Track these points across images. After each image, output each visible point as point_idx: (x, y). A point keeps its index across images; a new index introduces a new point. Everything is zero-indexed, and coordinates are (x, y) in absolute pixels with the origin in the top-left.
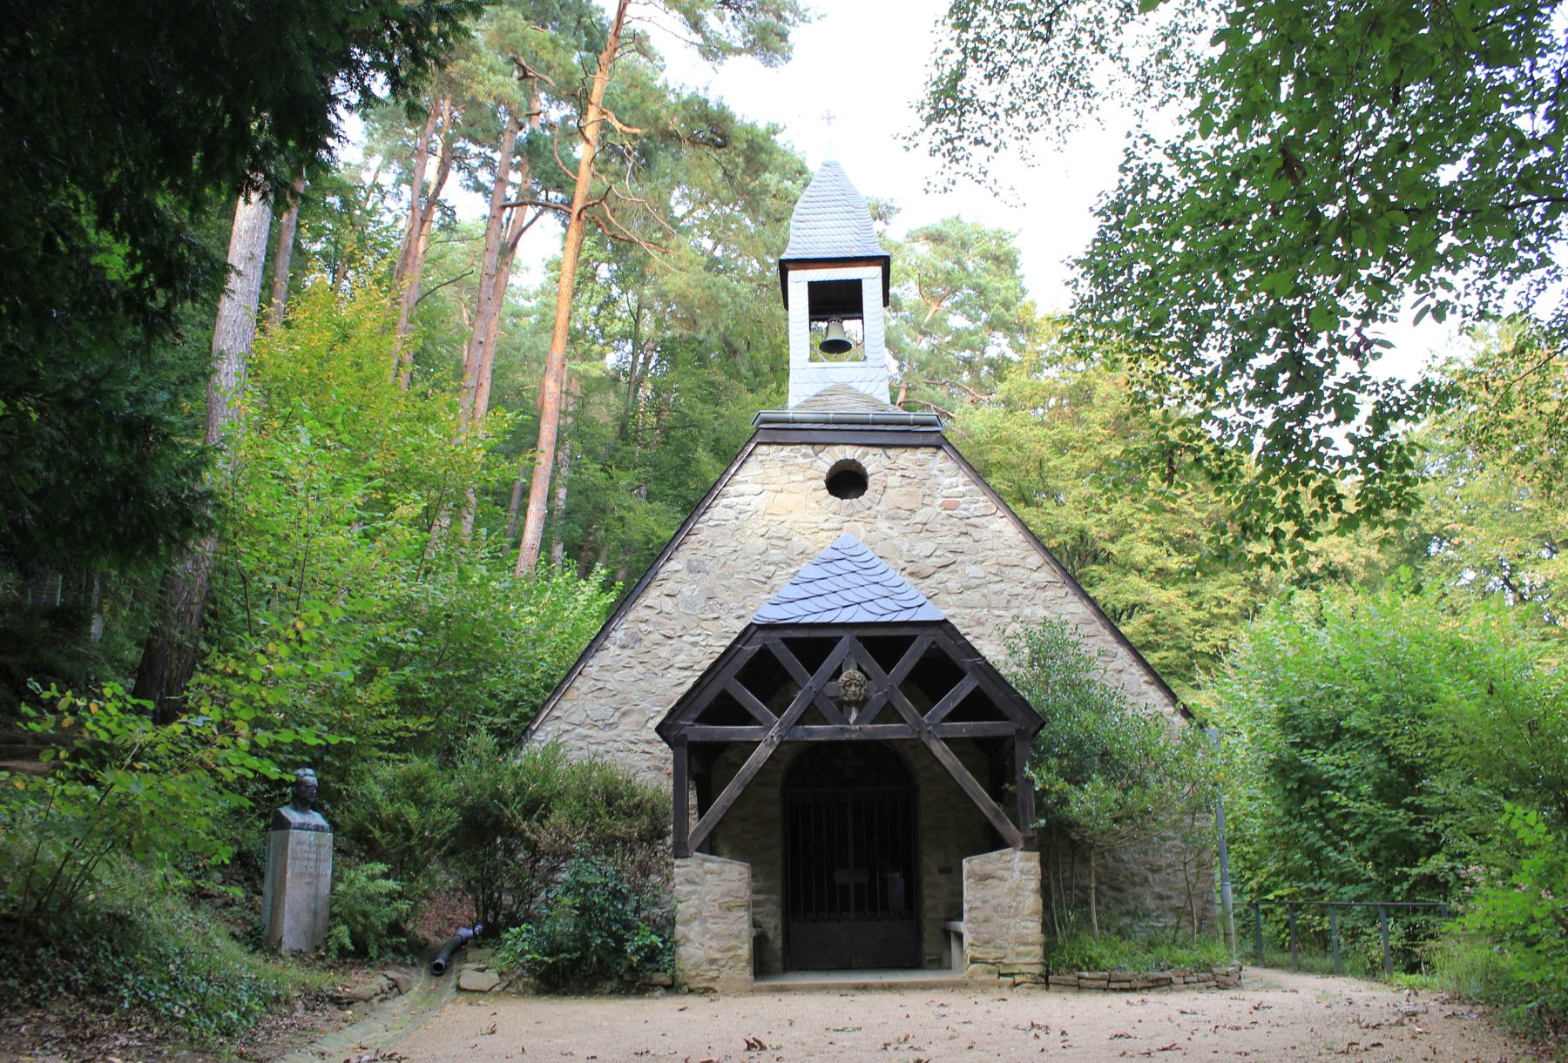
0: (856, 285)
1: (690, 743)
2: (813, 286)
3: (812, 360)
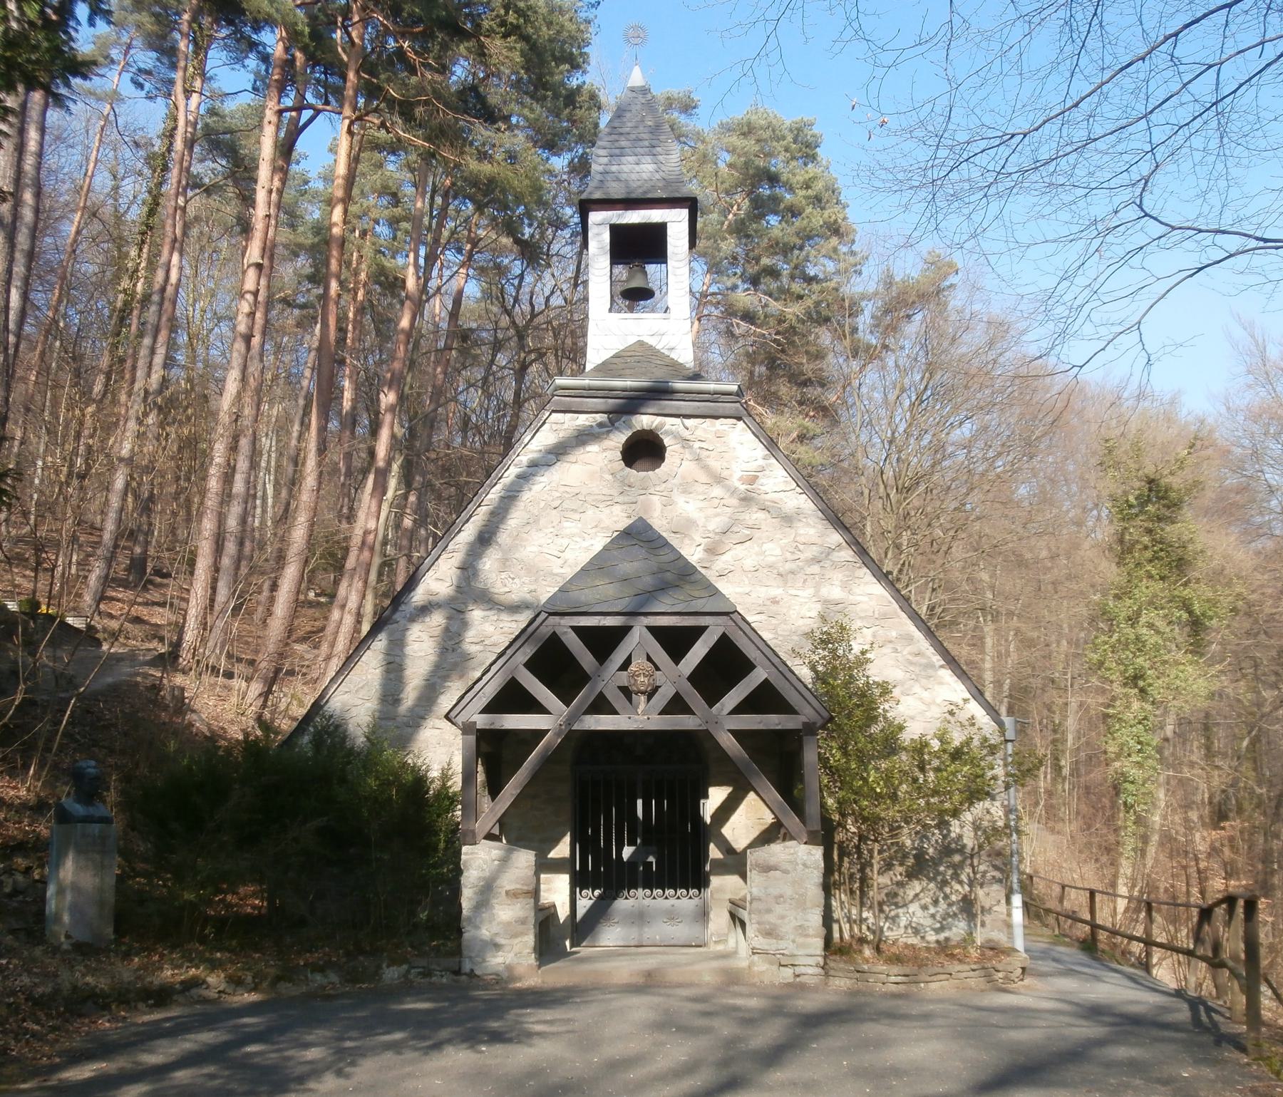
1: (478, 730)
3: (610, 310)
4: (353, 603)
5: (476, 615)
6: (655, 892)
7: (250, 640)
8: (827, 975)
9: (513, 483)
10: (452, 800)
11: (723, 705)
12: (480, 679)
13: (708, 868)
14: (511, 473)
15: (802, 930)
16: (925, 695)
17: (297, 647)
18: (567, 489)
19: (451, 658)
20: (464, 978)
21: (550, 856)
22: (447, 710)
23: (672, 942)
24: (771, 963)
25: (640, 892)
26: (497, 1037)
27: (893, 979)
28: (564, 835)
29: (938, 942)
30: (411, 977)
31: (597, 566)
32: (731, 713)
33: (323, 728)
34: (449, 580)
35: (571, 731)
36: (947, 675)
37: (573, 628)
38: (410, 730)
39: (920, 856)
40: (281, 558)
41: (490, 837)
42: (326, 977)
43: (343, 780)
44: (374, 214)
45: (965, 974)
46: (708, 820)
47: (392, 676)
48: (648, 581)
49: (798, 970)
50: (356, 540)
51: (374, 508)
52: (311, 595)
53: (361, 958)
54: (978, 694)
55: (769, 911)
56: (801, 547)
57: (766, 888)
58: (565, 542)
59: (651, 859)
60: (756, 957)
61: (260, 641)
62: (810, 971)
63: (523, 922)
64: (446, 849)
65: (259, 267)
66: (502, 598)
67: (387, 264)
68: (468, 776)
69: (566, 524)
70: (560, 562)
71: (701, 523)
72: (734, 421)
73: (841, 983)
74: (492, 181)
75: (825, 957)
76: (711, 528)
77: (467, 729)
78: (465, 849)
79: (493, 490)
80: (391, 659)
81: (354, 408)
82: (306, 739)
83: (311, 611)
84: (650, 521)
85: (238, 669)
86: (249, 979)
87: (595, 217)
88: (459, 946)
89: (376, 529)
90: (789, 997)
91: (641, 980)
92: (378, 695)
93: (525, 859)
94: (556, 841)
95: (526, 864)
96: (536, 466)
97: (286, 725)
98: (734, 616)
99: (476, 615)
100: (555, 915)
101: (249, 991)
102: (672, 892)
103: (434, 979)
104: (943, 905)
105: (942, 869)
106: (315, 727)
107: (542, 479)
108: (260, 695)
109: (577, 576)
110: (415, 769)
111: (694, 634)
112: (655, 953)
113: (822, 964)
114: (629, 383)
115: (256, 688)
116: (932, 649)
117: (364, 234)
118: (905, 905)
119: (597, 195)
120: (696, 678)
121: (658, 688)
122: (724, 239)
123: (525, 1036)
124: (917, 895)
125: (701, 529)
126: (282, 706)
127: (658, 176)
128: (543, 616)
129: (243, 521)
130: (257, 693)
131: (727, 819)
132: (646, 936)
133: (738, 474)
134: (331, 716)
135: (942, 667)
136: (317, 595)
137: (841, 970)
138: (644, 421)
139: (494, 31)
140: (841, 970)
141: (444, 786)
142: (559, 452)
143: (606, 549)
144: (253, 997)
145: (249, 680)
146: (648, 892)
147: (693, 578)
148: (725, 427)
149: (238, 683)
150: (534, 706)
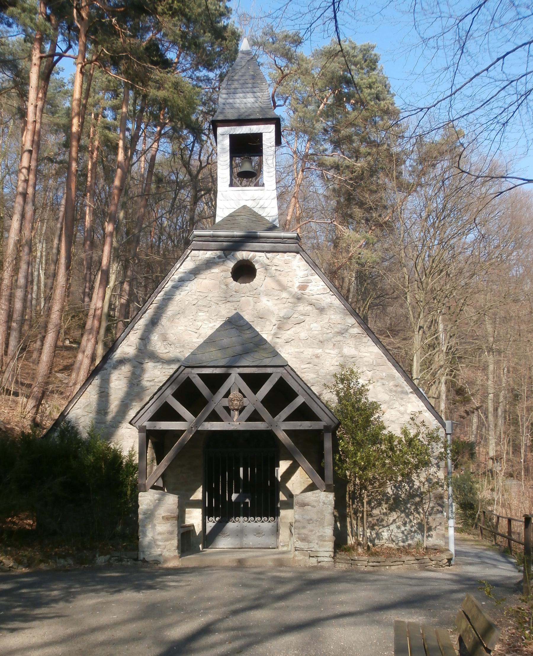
0: (258, 137)
1: (147, 430)
2: (234, 138)
3: (231, 185)
4: (89, 351)
5: (149, 365)
6: (250, 519)
7: (30, 371)
8: (335, 562)
9: (170, 290)
10: (135, 468)
11: (280, 416)
12: (148, 403)
13: (279, 506)
14: (168, 285)
15: (322, 538)
16: (402, 409)
17: (59, 375)
18: (201, 294)
19: (136, 389)
20: (140, 562)
21: (191, 499)
22: (130, 420)
23: (259, 546)
24: (305, 555)
25: (241, 519)
26: (150, 587)
27: (371, 564)
28: (199, 487)
29: (403, 547)
30: (111, 561)
31: (210, 341)
32: (285, 420)
33: (65, 428)
34: (135, 345)
35: (198, 432)
36: (414, 397)
37: (199, 375)
38: (113, 429)
39: (397, 498)
40: (45, 328)
41: (154, 487)
42: (66, 561)
43: (76, 457)
44: (103, 103)
45: (412, 562)
46: (279, 479)
47: (103, 399)
48: (239, 349)
49: (320, 559)
50: (91, 312)
51: (101, 294)
52: (67, 342)
53: (85, 552)
54: (433, 409)
55: (304, 527)
56: (332, 326)
57: (303, 515)
58: (200, 324)
59: (247, 500)
60: (297, 552)
61: (34, 371)
62: (326, 559)
63: (171, 533)
64: (131, 494)
65: (30, 152)
66: (161, 356)
67: (111, 136)
68: (142, 454)
69: (200, 314)
70: (197, 335)
71: (276, 313)
72: (295, 254)
73: (342, 566)
74: (165, 100)
75: (335, 552)
76: (281, 315)
77: (141, 429)
78: (140, 494)
79: (159, 295)
80: (103, 390)
81: (92, 227)
82: (56, 434)
83: (65, 353)
84: (242, 314)
85: (22, 390)
86: (26, 561)
87: (220, 130)
88: (137, 546)
89: (102, 307)
90: (308, 573)
91: (235, 564)
92: (96, 410)
93: (172, 500)
94: (194, 490)
95: (173, 502)
96: (182, 281)
97: (49, 424)
98: (286, 367)
99: (149, 365)
100: (194, 530)
101: (26, 567)
102: (259, 518)
103: (124, 563)
104: (408, 527)
105: (409, 505)
106: (60, 427)
107: (186, 288)
108: (34, 407)
109: (201, 346)
110: (115, 451)
111: (266, 377)
112: (248, 551)
113: (332, 556)
114: (236, 233)
115: (31, 403)
116: (405, 383)
117: (97, 116)
118: (388, 526)
119: (220, 118)
120: (266, 402)
121: (245, 407)
122: (317, 121)
123: (164, 587)
124: (394, 521)
125: (276, 316)
126: (48, 413)
127: (257, 105)
128: (182, 368)
129: (25, 300)
130: (32, 406)
131: (290, 478)
132: (244, 542)
133: (297, 284)
134: (69, 422)
135: (411, 392)
136: (71, 342)
137: (342, 559)
138: (242, 255)
139: (165, 13)
140: (342, 559)
141: (131, 461)
142: (195, 272)
143: (218, 330)
144: (25, 570)
145: (28, 397)
146: (246, 518)
147: (264, 347)
148: (290, 258)
149: (22, 399)
150: (177, 417)
